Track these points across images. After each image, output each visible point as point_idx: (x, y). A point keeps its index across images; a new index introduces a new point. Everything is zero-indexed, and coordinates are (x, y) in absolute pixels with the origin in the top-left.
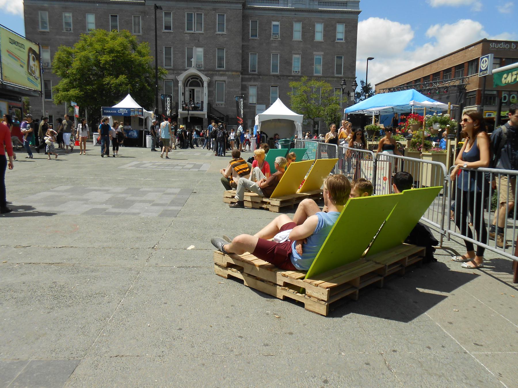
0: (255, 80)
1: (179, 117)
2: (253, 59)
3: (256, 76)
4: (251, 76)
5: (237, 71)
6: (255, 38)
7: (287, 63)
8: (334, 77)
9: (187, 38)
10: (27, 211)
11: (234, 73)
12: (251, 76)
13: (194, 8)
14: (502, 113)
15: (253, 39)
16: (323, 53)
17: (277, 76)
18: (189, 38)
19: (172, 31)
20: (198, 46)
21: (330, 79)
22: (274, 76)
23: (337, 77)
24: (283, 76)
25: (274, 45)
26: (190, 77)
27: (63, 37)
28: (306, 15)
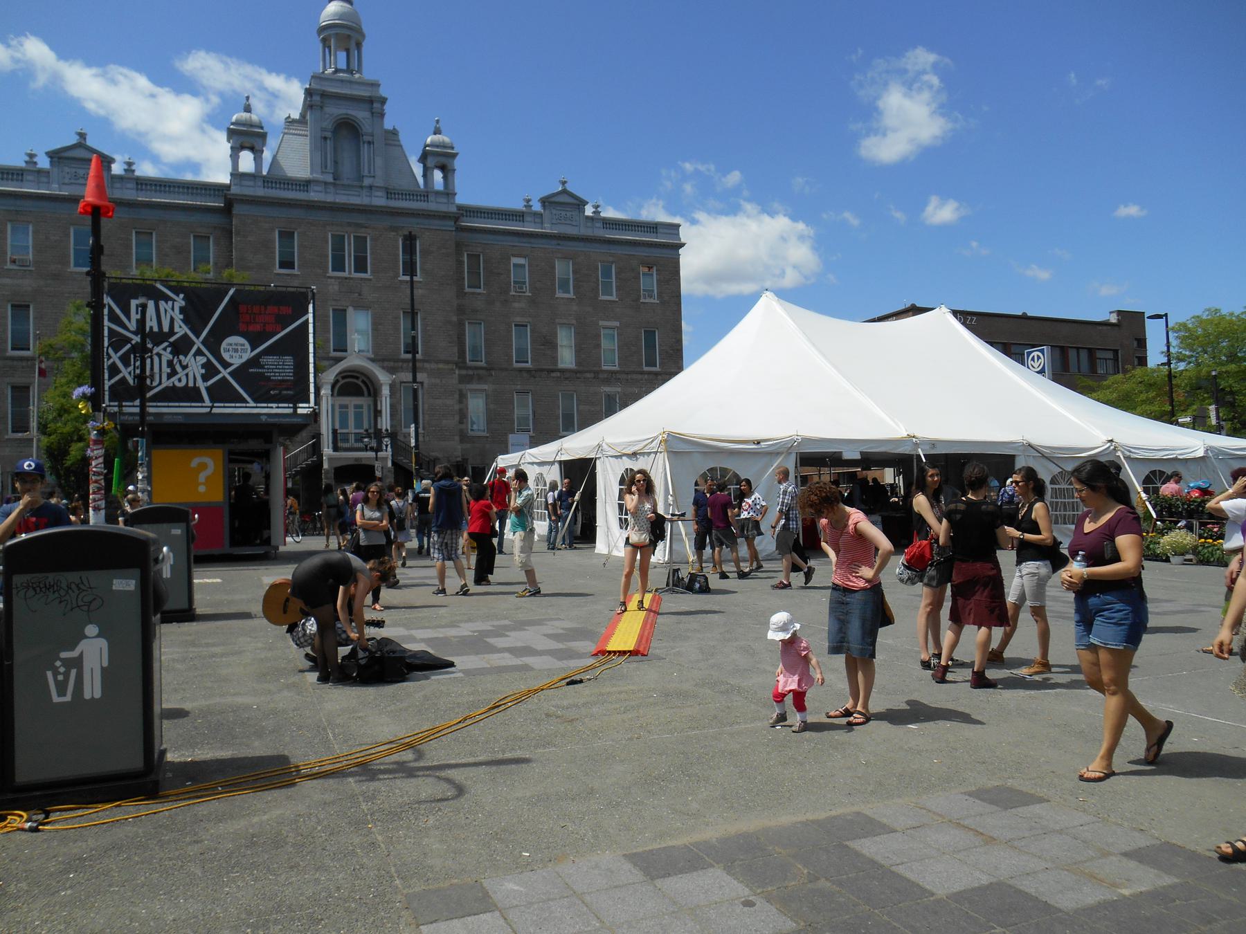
0: (480, 379)
1: (326, 466)
2: (474, 336)
3: (481, 372)
4: (471, 372)
5: (447, 362)
6: (478, 291)
7: (548, 344)
8: (642, 373)
9: (334, 287)
10: (660, 659)
11: (441, 366)
12: (471, 372)
13: (349, 224)
14: (137, 410)
15: (473, 293)
16: (617, 324)
17: (528, 371)
18: (336, 288)
19: (296, 271)
20: (359, 306)
21: (635, 376)
22: (521, 370)
23: (649, 373)
24: (542, 370)
25: (516, 305)
26: (365, 375)
27: (7, 281)
28: (580, 247)
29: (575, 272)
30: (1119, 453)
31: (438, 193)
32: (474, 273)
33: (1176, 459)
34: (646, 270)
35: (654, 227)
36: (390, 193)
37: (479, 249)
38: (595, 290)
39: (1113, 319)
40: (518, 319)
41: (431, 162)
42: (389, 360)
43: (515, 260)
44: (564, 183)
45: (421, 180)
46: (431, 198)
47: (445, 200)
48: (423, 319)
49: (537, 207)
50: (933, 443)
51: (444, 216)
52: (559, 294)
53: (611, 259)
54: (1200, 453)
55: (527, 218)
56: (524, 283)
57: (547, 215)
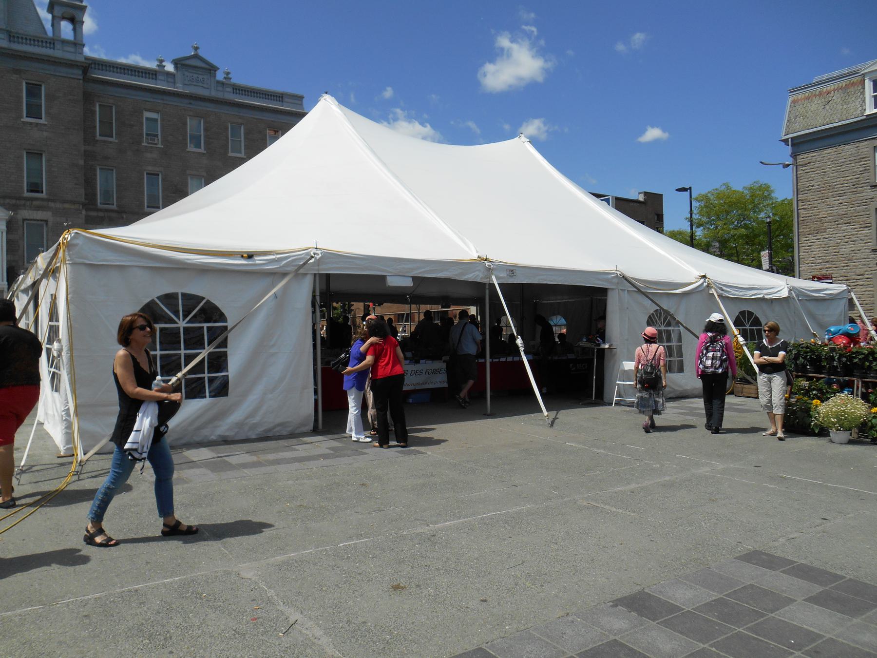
4: (101, 214)
5: (73, 202)
6: (110, 139)
11: (67, 206)
12: (101, 214)
15: (105, 141)
25: (148, 155)
28: (211, 108)
29: (205, 130)
30: (712, 291)
31: (64, 42)
32: (106, 124)
33: (763, 299)
34: (272, 133)
35: (279, 97)
36: (12, 36)
37: (111, 101)
38: (225, 147)
39: (641, 198)
40: (150, 168)
41: (58, 11)
42: (10, 197)
43: (147, 114)
44: (196, 49)
45: (48, 26)
46: (58, 46)
47: (72, 50)
48: (48, 161)
49: (170, 68)
50: (512, 269)
51: (72, 64)
52: (191, 148)
53: (240, 121)
54: (785, 294)
55: (160, 77)
56: (157, 136)
57: (179, 76)
